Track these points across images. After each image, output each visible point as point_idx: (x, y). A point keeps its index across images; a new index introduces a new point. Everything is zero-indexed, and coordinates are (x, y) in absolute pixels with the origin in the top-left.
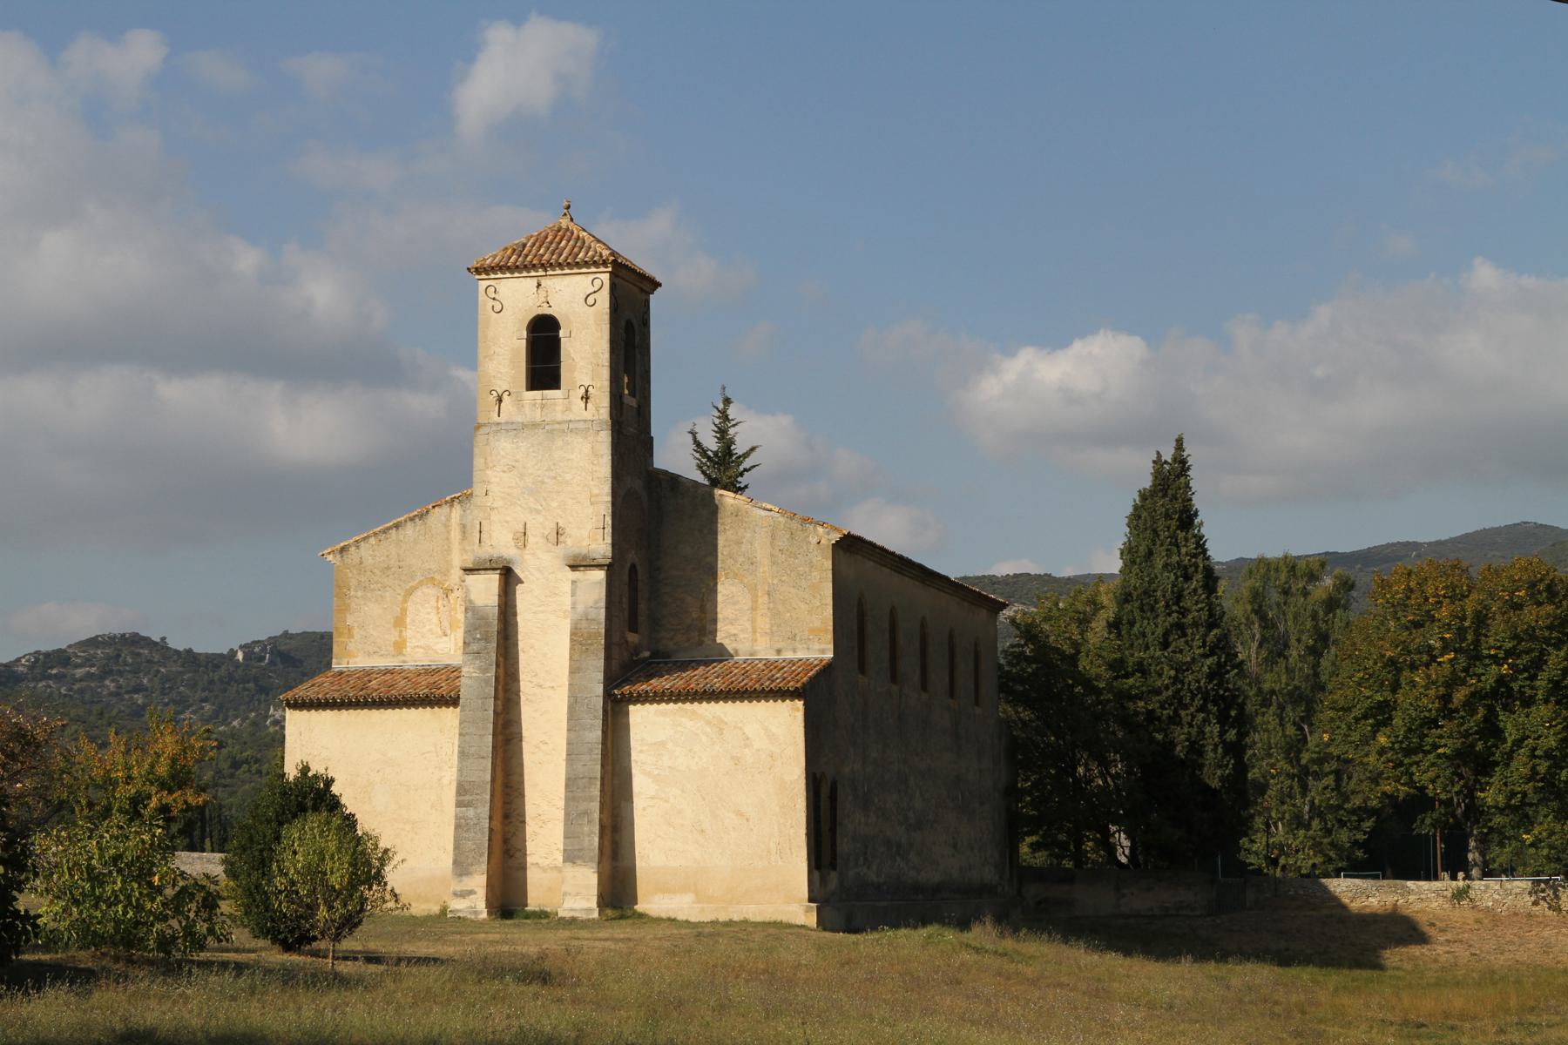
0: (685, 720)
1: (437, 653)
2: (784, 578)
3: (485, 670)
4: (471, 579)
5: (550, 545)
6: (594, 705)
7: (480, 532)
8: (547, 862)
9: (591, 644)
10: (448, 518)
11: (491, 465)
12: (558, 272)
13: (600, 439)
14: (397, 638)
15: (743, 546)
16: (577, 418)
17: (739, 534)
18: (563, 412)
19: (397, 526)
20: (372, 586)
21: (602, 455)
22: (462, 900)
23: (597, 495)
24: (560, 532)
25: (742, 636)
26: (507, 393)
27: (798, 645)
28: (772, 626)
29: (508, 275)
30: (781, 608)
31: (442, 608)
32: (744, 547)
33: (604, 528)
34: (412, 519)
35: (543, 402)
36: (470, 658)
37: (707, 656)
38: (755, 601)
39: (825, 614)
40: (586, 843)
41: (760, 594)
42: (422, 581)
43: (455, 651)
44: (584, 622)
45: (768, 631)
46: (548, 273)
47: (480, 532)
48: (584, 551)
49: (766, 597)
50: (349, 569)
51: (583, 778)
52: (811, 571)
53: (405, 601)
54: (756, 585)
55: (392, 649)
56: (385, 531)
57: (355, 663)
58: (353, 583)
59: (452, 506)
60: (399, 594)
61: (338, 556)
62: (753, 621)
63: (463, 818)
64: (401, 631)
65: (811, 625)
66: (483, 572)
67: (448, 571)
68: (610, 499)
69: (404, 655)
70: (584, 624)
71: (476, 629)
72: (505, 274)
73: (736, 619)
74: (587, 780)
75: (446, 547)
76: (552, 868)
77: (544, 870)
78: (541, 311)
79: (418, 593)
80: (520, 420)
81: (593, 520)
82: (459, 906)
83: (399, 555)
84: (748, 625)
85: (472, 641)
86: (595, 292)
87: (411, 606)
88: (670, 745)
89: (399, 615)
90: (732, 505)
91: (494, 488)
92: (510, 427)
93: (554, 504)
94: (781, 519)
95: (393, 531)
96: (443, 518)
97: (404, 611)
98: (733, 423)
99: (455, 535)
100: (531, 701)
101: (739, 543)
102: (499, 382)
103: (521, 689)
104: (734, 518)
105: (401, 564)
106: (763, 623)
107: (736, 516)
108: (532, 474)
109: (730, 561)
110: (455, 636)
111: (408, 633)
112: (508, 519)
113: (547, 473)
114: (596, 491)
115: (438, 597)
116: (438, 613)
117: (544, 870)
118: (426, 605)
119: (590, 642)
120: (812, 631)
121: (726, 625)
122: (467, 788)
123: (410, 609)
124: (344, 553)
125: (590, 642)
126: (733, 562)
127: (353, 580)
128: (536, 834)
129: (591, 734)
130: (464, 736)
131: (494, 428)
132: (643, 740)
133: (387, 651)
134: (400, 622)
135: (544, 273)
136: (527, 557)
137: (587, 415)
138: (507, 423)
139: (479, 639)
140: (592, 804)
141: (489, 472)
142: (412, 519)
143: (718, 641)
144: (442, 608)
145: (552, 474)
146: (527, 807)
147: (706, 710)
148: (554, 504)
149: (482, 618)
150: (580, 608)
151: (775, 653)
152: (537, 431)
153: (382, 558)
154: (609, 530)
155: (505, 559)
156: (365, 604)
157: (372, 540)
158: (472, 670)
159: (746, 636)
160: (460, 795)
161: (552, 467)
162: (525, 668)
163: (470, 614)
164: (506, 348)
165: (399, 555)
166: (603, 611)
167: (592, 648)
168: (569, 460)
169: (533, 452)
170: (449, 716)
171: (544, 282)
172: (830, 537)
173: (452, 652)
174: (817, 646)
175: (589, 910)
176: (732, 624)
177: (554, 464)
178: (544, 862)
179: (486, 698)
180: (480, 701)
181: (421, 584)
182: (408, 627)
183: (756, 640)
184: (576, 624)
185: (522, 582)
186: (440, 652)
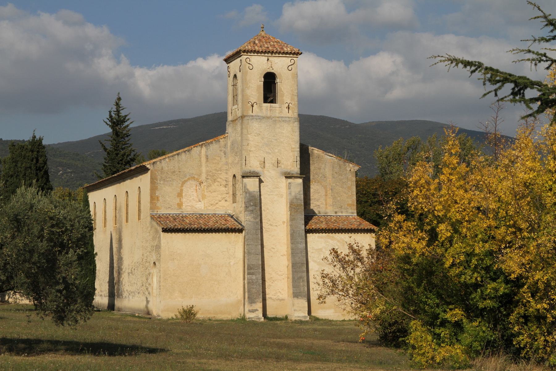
1: (197, 209)
2: (337, 184)
3: (255, 218)
4: (246, 180)
8: (275, 297)
9: (298, 209)
10: (200, 152)
11: (250, 133)
12: (277, 55)
13: (295, 125)
16: (285, 116)
17: (320, 165)
18: (279, 113)
19: (178, 154)
21: (296, 132)
22: (253, 313)
23: (294, 148)
24: (279, 162)
25: (321, 206)
26: (256, 103)
27: (343, 210)
28: (333, 202)
29: (256, 54)
30: (336, 195)
31: (198, 190)
32: (322, 171)
33: (297, 162)
35: (271, 108)
36: (249, 213)
37: (308, 214)
38: (326, 192)
40: (302, 289)
41: (328, 189)
43: (204, 208)
44: (295, 200)
45: (331, 204)
48: (289, 171)
50: (157, 171)
51: (299, 263)
52: (347, 181)
53: (182, 186)
55: (177, 206)
56: (172, 156)
57: (161, 212)
58: (159, 177)
59: (202, 147)
60: (179, 183)
62: (326, 200)
64: (180, 199)
65: (348, 203)
66: (252, 177)
67: (201, 174)
69: (182, 209)
70: (295, 201)
71: (251, 201)
72: (251, 53)
73: (319, 199)
74: (300, 264)
75: (199, 164)
76: (277, 300)
79: (188, 183)
80: (261, 115)
82: (249, 315)
83: (179, 167)
84: (324, 202)
86: (291, 65)
87: (184, 188)
88: (324, 250)
89: (179, 192)
90: (317, 154)
93: (277, 151)
94: (336, 160)
96: (198, 152)
97: (182, 190)
98: (122, 108)
99: (204, 159)
100: (268, 231)
101: (320, 169)
102: (252, 99)
103: (263, 226)
105: (180, 170)
106: (330, 201)
108: (267, 138)
111: (184, 200)
112: (257, 155)
113: (273, 138)
114: (293, 146)
116: (197, 192)
118: (191, 188)
119: (298, 208)
120: (348, 205)
121: (315, 201)
124: (155, 164)
127: (158, 176)
128: (270, 285)
130: (249, 245)
131: (251, 118)
132: (313, 248)
134: (180, 195)
135: (271, 55)
136: (265, 172)
137: (289, 115)
138: (256, 116)
139: (252, 205)
141: (249, 136)
142: (185, 152)
143: (311, 208)
144: (198, 190)
145: (275, 138)
147: (338, 236)
148: (277, 151)
149: (253, 197)
150: (293, 194)
151: (334, 213)
152: (269, 120)
153: (172, 168)
154: (299, 162)
155: (256, 172)
156: (164, 187)
157: (167, 160)
158: (250, 218)
159: (323, 206)
160: (249, 270)
161: (275, 135)
163: (248, 195)
165: (179, 167)
166: (302, 196)
167: (299, 210)
168: (282, 133)
170: (238, 238)
171: (270, 59)
172: (355, 168)
173: (203, 208)
174: (350, 211)
175: (305, 317)
181: (189, 179)
182: (184, 197)
185: (263, 182)
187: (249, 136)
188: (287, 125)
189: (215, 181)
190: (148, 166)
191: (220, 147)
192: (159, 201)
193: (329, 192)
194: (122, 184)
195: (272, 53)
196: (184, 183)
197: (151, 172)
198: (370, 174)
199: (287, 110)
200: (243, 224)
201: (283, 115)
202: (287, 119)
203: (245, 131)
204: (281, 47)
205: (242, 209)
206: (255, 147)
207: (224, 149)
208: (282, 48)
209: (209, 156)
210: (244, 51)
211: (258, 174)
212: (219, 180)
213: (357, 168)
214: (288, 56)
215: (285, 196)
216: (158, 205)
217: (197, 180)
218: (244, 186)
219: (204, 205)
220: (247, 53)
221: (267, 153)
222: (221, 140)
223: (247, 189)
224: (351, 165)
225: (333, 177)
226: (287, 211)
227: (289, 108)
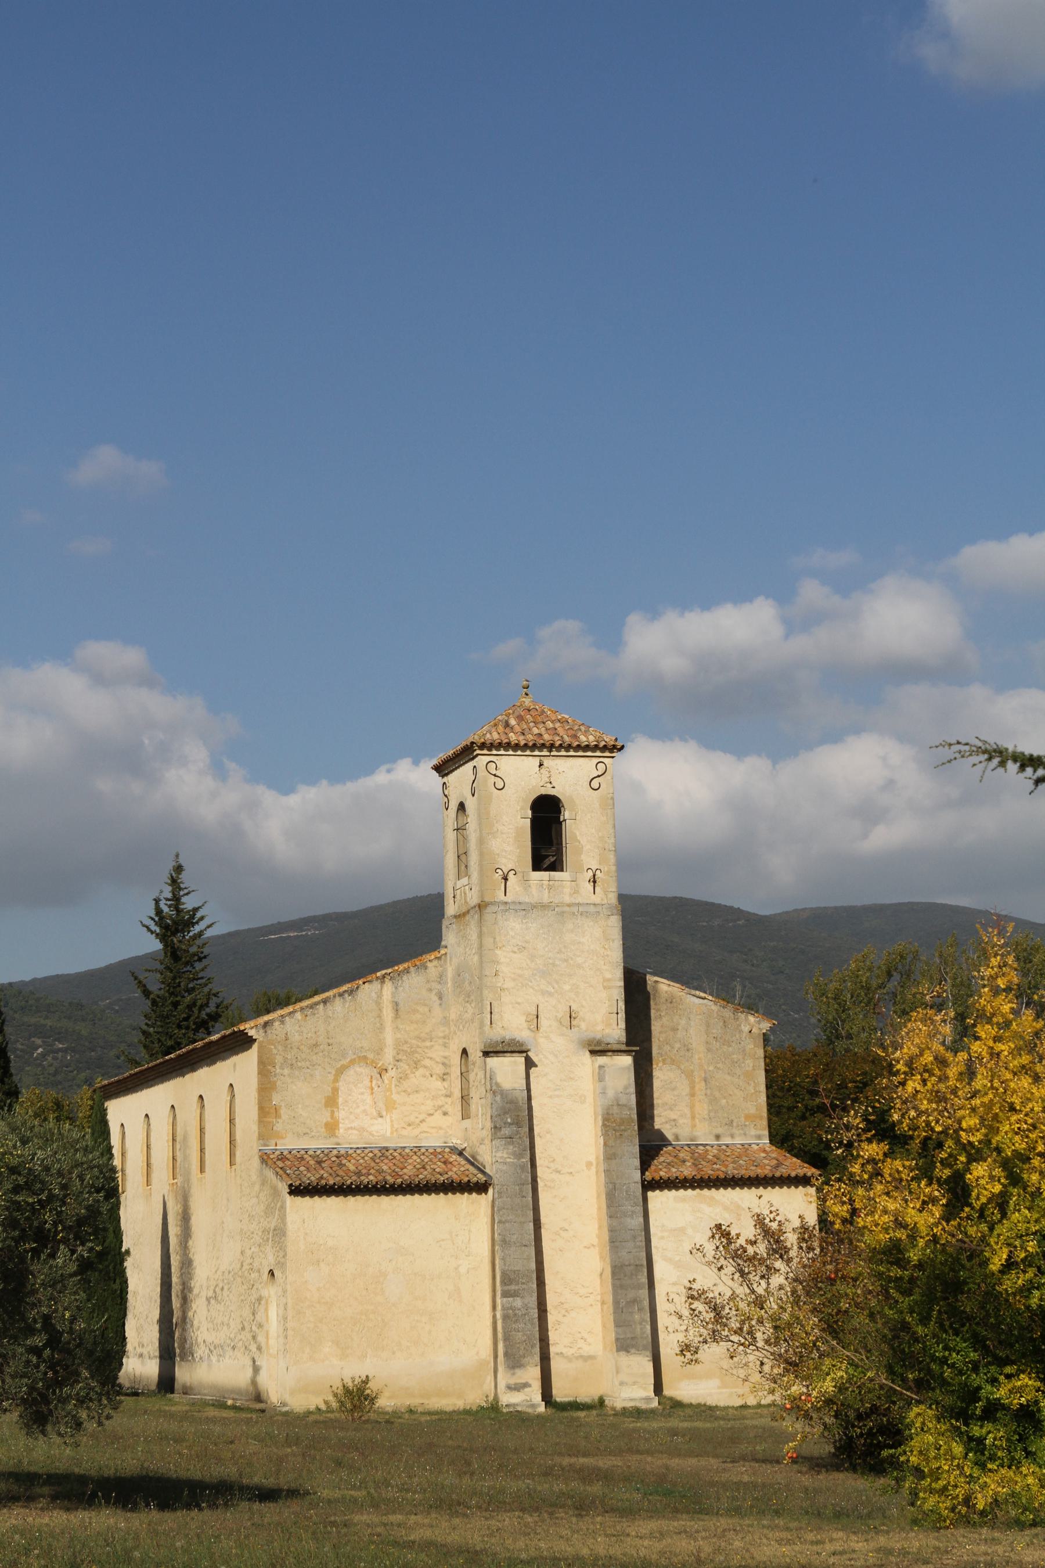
0: (704, 1207)
1: (373, 1135)
2: (718, 1066)
4: (493, 1062)
5: (564, 1028)
6: (634, 1192)
7: (491, 1013)
8: (571, 1351)
9: (625, 1130)
10: (380, 996)
11: (500, 945)
12: (563, 753)
14: (329, 1119)
15: (679, 1032)
16: (586, 901)
19: (325, 1002)
20: (299, 1064)
21: (613, 941)
22: (517, 1393)
23: (609, 980)
24: (573, 1015)
25: (681, 1121)
26: (513, 872)
27: (735, 1131)
30: (717, 1094)
32: (680, 1034)
33: (617, 1013)
34: (341, 995)
35: (551, 883)
38: (692, 1088)
39: (759, 1101)
41: (697, 1080)
42: (355, 1059)
44: (615, 1108)
46: (552, 754)
47: (491, 1013)
48: (598, 1036)
49: (703, 1083)
50: (272, 1044)
52: (744, 1058)
54: (692, 1071)
55: (323, 1130)
56: (311, 1007)
58: (279, 1059)
59: (383, 982)
61: (261, 1031)
62: (692, 1107)
63: (511, 1308)
64: (333, 1112)
65: (746, 1112)
66: (509, 1054)
68: (622, 984)
69: (336, 1137)
71: (505, 1113)
74: (632, 1267)
76: (577, 1358)
77: (569, 1359)
78: (544, 791)
80: (527, 900)
81: (607, 1005)
82: (509, 1399)
84: (687, 1111)
85: (503, 1125)
86: (599, 776)
87: (342, 1085)
88: (690, 1231)
89: (330, 1094)
90: (666, 992)
91: (504, 969)
92: (518, 907)
93: (567, 987)
94: (714, 1007)
95: (321, 1006)
96: (373, 995)
97: (335, 1090)
98: (186, 891)
99: (388, 1013)
101: (675, 1030)
102: (504, 861)
104: (669, 1005)
105: (330, 1041)
106: (702, 1108)
107: (671, 1003)
108: (543, 956)
109: (667, 1048)
110: (391, 1117)
111: (341, 1114)
112: (519, 1000)
114: (608, 976)
115: (372, 1077)
117: (569, 1359)
119: (623, 1127)
120: (748, 1117)
121: (665, 1110)
122: (512, 1277)
123: (342, 1088)
125: (623, 1127)
126: (669, 1048)
128: (559, 1323)
129: (633, 1221)
130: (504, 1223)
131: (502, 907)
133: (318, 1132)
134: (331, 1102)
135: (548, 754)
136: (541, 1040)
137: (596, 899)
138: (514, 903)
139: (510, 1124)
140: (640, 1291)
141: (498, 952)
142: (341, 995)
146: (548, 1296)
147: (724, 1196)
148: (567, 987)
149: (511, 1102)
150: (611, 1093)
151: (713, 1138)
154: (622, 1015)
155: (518, 1042)
157: (298, 1015)
158: (505, 1156)
159: (686, 1121)
161: (563, 950)
162: (542, 1153)
163: (498, 1098)
164: (511, 827)
165: (328, 1032)
168: (579, 943)
169: (544, 933)
170: (477, 1206)
171: (547, 762)
172: (761, 1026)
173: (388, 1134)
174: (753, 1132)
175: (648, 1399)
176: (671, 1109)
177: (565, 947)
178: (569, 1352)
179: (523, 1184)
180: (517, 1188)
181: (352, 1062)
182: (341, 1107)
183: (695, 1126)
184: (608, 1109)
185: (536, 1066)
186: (375, 1134)
187: (498, 952)
188: (592, 923)
189: (416, 1065)
190: (252, 1033)
191: (428, 981)
192: (280, 1117)
193: (700, 1086)
194: (187, 1076)
195: (551, 747)
196: (340, 1071)
197: (259, 1048)
198: (799, 1037)
199: (590, 886)
200: (488, 1171)
201: (580, 900)
202: (592, 909)
203: (488, 941)
204: (571, 732)
205: (486, 1133)
206: (514, 980)
207: (439, 987)
208: (575, 737)
209: (401, 1005)
210: (483, 746)
211: (522, 1045)
212: (427, 1062)
213: (766, 1026)
214: (589, 754)
215: (590, 1099)
216: (279, 1127)
217: (373, 1064)
218: (488, 1076)
219: (392, 1126)
220: (490, 750)
221: (544, 993)
222: (429, 964)
223: (497, 1084)
224: (751, 1019)
225: (709, 1050)
226: (596, 1135)
227: (595, 882)
